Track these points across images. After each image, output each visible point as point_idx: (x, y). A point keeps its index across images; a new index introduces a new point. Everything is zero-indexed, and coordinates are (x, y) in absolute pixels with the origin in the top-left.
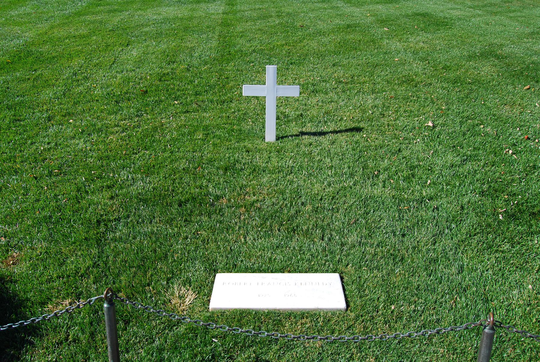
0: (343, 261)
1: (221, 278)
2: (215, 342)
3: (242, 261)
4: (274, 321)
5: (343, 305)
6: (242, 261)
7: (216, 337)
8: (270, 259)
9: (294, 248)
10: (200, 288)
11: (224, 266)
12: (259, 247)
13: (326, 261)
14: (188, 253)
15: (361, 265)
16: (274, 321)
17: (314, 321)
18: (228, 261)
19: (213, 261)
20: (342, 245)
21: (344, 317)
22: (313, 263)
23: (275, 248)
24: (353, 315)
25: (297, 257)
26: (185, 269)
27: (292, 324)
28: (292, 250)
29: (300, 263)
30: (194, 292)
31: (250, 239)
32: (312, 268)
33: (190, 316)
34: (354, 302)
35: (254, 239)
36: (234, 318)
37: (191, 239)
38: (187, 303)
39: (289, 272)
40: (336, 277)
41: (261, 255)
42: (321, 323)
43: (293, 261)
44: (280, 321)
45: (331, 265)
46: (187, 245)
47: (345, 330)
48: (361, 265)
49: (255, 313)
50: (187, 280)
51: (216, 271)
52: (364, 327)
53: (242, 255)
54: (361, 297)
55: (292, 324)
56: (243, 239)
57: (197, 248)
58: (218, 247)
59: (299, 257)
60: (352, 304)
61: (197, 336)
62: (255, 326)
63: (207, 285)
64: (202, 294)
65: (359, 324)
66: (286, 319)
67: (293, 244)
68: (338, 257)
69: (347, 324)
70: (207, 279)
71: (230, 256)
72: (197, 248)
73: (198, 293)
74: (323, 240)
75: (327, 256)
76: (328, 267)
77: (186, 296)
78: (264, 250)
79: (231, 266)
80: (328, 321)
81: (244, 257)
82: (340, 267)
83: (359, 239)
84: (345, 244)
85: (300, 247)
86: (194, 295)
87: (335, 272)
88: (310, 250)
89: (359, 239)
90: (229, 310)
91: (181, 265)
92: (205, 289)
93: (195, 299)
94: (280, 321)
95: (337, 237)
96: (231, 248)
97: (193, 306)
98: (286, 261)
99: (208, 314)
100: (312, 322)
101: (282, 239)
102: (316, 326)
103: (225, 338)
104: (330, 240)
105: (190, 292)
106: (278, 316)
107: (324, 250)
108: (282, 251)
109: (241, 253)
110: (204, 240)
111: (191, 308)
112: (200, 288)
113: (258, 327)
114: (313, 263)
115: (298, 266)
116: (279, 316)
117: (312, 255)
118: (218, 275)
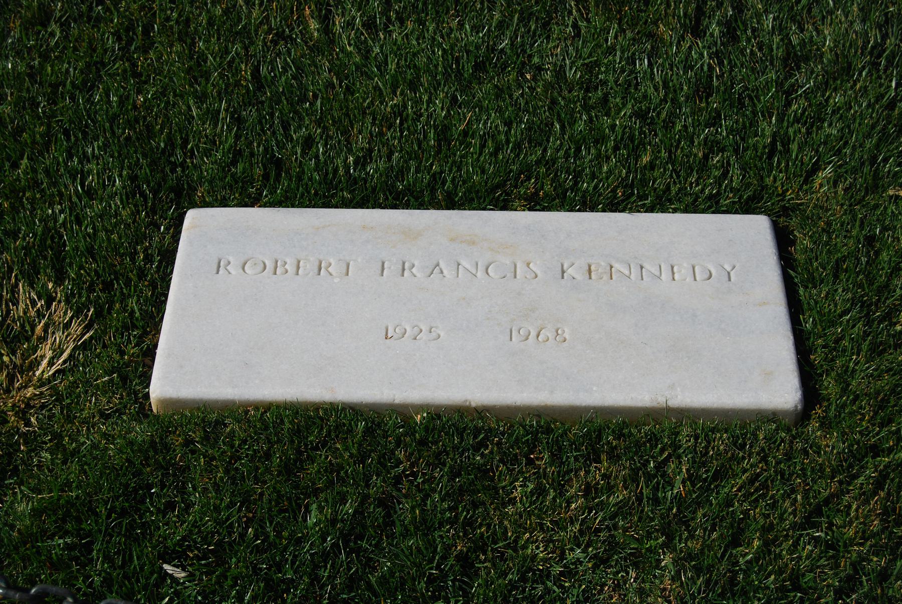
0: (794, 147)
1: (209, 235)
2: (174, 580)
3: (308, 142)
4: (454, 474)
5: (782, 391)
6: (308, 142)
7: (176, 556)
8: (443, 133)
9: (560, 73)
10: (108, 287)
11: (225, 168)
12: (392, 67)
13: (713, 146)
14: (53, 100)
15: (876, 176)
16: (454, 474)
17: (649, 477)
18: (242, 144)
19: (170, 141)
20: (794, 59)
21: (789, 456)
22: (646, 159)
23: (469, 70)
24: (832, 444)
25: (573, 122)
26: (35, 184)
27: (540, 491)
28: (548, 86)
29: (588, 156)
30: (76, 315)
31: (350, 24)
32: (644, 182)
33: (58, 437)
34: (839, 379)
35: (370, 25)
36: (268, 456)
37: (64, 26)
38: (43, 370)
39: (534, 203)
40: (756, 229)
41: (399, 111)
42: (678, 488)
43: (553, 143)
44: (484, 472)
45: (735, 173)
46: (45, 57)
47: (794, 526)
48: (876, 176)
49: (368, 431)
50: (43, 246)
51: (186, 198)
52: (886, 512)
53: (311, 112)
54: (877, 350)
55: (540, 491)
56: (313, 25)
57: (95, 69)
58: (197, 70)
59: (580, 126)
60: (829, 386)
61: (88, 547)
62: (365, 498)
63: (142, 275)
64: (116, 317)
65: (865, 497)
66: (515, 460)
67: (555, 52)
68: (767, 128)
69: (806, 497)
70: (139, 239)
71: (250, 114)
72: (95, 69)
73: (99, 314)
74: (698, 31)
75: (715, 121)
76: (719, 181)
77: (39, 329)
78: (413, 86)
79: (258, 171)
80: (715, 477)
81: (319, 123)
82: (776, 179)
83: (874, 36)
84: (807, 59)
85: (589, 68)
86: (76, 328)
87: (747, 207)
88: (629, 86)
89: (874, 36)
90: (257, 406)
91: (15, 166)
92: (129, 297)
93: (85, 346)
94: (484, 472)
95: (769, 22)
96: (256, 72)
97: (74, 385)
98: (518, 146)
99: (140, 432)
100: (636, 480)
101: (501, 25)
102: (656, 501)
103: (221, 562)
104: (731, 32)
105: (61, 312)
106: (477, 448)
107: (703, 89)
108: (499, 92)
109: (303, 99)
110: (131, 28)
111: (64, 396)
112: (108, 287)
113: (381, 503)
114: (646, 159)
115: (578, 176)
116: (482, 444)
117: (641, 115)
118: (198, 222)
